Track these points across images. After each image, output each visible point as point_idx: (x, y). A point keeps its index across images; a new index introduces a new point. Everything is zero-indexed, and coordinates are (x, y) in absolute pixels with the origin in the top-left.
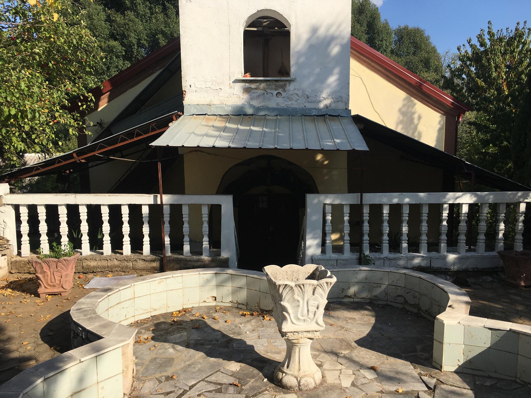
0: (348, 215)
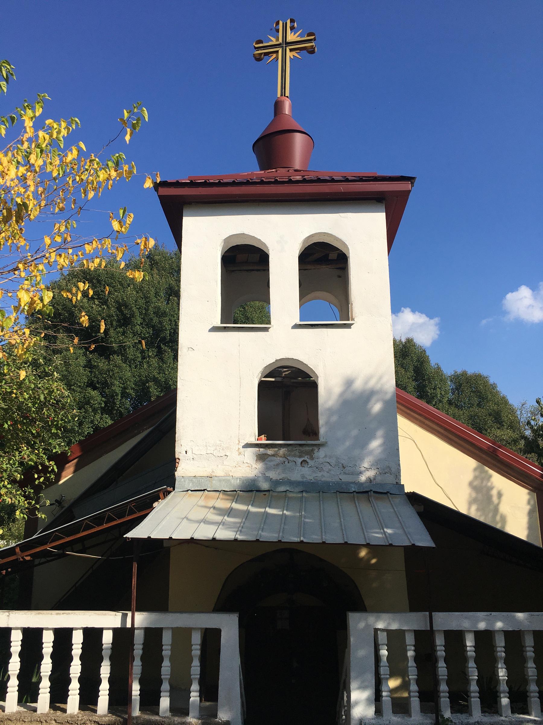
0: (413, 648)
